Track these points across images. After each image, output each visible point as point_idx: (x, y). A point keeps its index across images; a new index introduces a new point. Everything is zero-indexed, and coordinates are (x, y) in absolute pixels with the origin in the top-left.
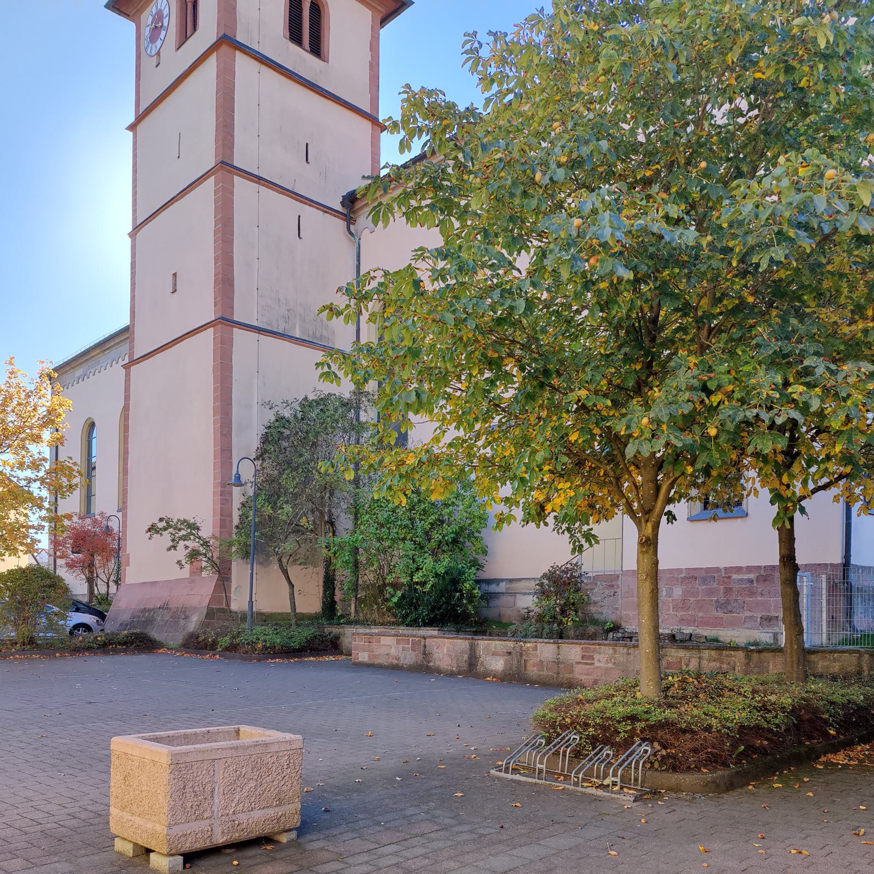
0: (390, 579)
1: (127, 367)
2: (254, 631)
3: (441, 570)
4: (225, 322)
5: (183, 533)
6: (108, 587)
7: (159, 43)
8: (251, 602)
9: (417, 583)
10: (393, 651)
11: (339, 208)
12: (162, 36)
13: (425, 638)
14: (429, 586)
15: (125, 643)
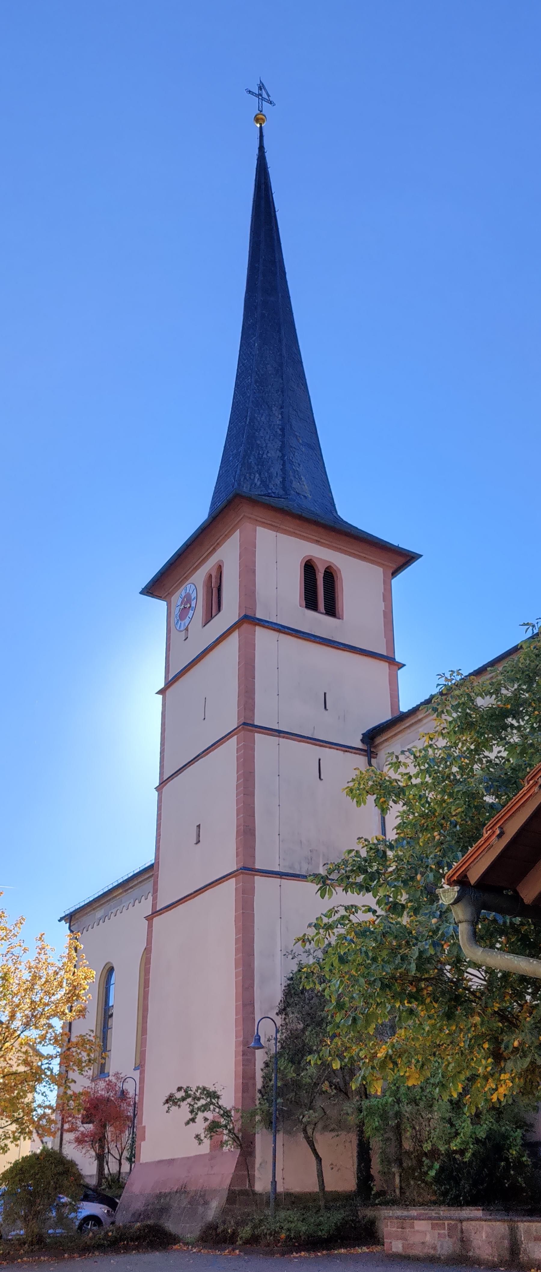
0: (427, 1147)
1: (149, 918)
2: (277, 1218)
3: (482, 1135)
4: (247, 871)
5: (203, 1102)
6: (120, 1164)
7: (187, 620)
8: (274, 1183)
9: (455, 1152)
10: (428, 1238)
11: (360, 745)
12: (190, 615)
13: (461, 1221)
14: (468, 1155)
15: (138, 1238)
